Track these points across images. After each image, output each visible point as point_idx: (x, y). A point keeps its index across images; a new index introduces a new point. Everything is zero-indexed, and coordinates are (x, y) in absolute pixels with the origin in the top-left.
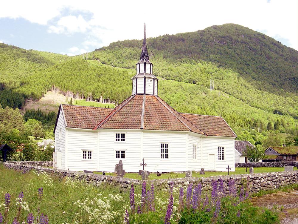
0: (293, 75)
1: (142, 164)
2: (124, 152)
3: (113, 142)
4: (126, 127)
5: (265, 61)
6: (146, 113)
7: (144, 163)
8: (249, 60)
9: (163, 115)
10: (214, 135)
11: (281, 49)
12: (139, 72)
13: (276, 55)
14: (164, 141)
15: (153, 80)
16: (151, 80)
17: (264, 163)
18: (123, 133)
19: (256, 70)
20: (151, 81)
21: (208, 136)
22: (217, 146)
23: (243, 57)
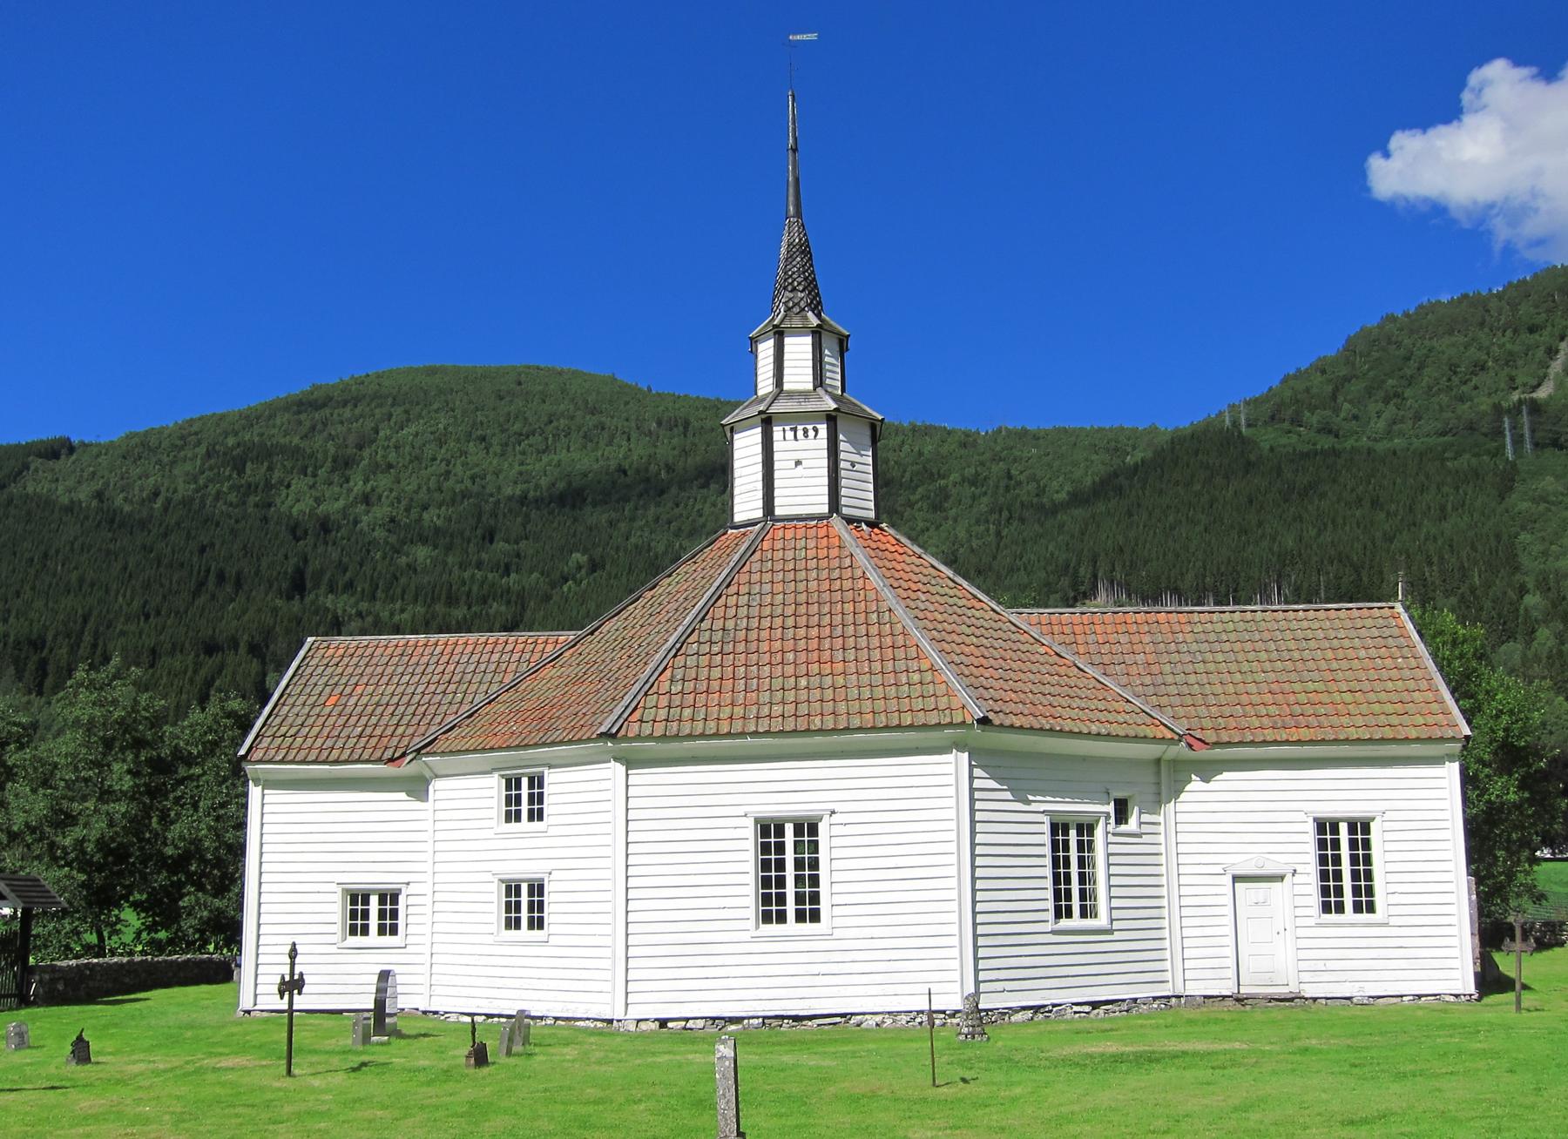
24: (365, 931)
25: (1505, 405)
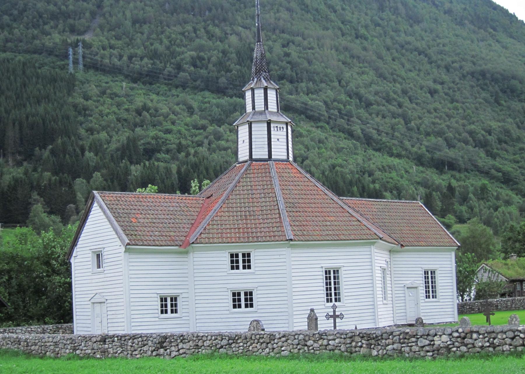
0: (480, 65)
1: (338, 316)
2: (251, 294)
3: (225, 274)
4: (253, 237)
5: (405, 27)
6: (288, 205)
7: (337, 313)
8: (366, 27)
9: (319, 205)
10: (416, 243)
12: (254, 108)
13: (434, 9)
15: (285, 126)
17: (497, 301)
18: (246, 251)
19: (384, 52)
20: (282, 129)
21: (406, 248)
23: (348, 16)
24: (166, 312)
25: (69, 41)
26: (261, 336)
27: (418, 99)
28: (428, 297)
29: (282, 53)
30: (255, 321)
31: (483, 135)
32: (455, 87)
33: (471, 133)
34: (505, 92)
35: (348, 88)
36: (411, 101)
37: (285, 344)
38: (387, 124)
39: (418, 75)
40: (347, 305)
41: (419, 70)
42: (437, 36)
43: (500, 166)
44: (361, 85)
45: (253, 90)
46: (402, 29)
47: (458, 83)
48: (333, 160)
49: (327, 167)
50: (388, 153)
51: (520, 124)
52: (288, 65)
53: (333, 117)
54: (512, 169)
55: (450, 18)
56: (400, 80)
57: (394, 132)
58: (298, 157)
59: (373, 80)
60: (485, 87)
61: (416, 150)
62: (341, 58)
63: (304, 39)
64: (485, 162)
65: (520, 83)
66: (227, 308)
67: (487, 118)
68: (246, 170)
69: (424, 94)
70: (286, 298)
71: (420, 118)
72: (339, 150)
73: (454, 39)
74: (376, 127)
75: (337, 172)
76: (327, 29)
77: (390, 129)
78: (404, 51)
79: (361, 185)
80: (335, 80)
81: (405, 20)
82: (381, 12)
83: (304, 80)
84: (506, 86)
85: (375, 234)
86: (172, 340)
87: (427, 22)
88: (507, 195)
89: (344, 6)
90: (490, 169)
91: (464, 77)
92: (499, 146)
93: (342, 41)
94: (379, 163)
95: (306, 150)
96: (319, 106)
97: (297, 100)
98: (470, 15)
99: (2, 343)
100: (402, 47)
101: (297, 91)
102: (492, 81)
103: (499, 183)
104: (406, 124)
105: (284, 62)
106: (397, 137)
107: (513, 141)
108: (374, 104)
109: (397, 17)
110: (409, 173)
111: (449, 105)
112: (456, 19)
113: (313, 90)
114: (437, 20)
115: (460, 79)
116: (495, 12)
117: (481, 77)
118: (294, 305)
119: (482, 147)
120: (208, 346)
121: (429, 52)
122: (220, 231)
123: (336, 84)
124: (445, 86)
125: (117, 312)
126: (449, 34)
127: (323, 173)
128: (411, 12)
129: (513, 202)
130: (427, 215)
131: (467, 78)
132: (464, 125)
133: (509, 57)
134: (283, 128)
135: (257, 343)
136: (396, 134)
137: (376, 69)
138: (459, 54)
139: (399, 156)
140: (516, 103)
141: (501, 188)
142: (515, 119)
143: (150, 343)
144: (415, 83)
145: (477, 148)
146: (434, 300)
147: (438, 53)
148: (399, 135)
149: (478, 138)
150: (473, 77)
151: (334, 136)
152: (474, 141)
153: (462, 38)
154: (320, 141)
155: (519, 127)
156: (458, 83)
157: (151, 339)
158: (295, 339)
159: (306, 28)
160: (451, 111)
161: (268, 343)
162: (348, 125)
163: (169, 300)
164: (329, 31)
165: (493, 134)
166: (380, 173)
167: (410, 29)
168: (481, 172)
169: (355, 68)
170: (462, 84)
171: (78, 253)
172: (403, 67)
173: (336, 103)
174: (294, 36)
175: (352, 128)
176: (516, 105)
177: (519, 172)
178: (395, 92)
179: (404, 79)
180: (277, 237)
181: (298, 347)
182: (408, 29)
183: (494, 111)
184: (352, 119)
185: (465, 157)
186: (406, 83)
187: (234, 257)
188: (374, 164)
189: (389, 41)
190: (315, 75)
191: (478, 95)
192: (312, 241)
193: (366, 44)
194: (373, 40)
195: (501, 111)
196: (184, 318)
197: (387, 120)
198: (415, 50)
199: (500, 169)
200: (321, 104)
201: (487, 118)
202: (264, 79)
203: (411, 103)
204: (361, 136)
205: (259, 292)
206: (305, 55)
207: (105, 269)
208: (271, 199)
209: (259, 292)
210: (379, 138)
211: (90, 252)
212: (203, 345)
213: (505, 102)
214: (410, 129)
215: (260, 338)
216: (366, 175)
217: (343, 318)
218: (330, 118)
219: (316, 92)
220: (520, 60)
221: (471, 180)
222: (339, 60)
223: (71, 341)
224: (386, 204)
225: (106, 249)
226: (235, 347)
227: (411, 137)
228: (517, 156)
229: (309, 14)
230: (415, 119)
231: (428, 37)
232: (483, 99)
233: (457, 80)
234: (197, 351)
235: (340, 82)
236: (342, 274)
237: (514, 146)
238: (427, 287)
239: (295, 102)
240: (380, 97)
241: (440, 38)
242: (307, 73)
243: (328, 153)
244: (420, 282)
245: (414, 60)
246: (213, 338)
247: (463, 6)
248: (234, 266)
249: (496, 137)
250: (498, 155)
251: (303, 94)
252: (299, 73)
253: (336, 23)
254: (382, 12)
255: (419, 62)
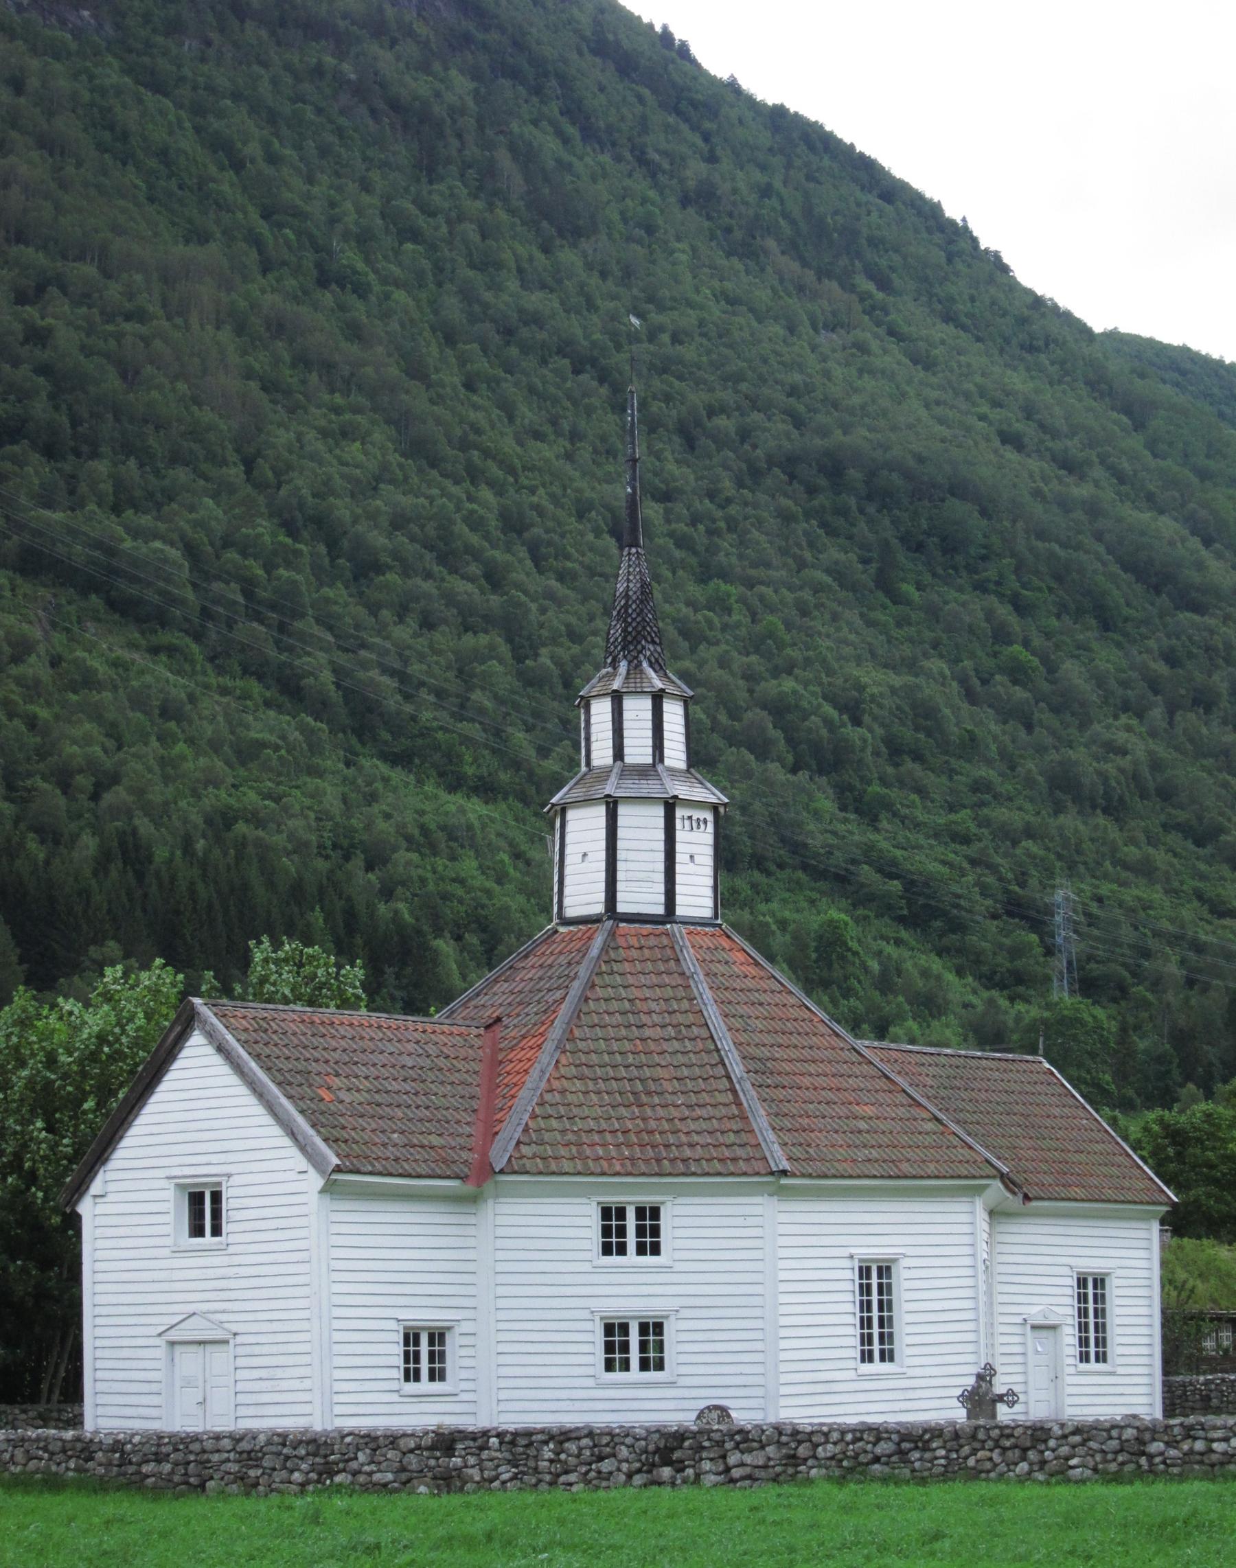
0: (823, 432)
2: (659, 1328)
4: (672, 1161)
5: (521, 250)
8: (363, 239)
11: (695, 128)
13: (640, 184)
14: (1092, 1265)
16: (698, 814)
17: (1207, 1383)
18: (647, 1199)
19: (431, 350)
21: (1034, 1204)
22: (1066, 1271)
26: (1007, 1431)
27: (568, 557)
28: (1085, 1358)
29: (18, 327)
30: (717, 1407)
31: (828, 722)
32: (719, 514)
33: (779, 709)
34: (919, 548)
35: (283, 492)
36: (537, 560)
37: (1081, 1450)
38: (438, 652)
39: (569, 457)
40: (910, 1372)
41: (575, 436)
42: (651, 299)
43: (899, 853)
44: (338, 482)
45: (617, 699)
46: (507, 256)
47: (729, 501)
48: (223, 794)
49: (196, 818)
50: (441, 774)
51: (975, 682)
52: (41, 380)
53: (221, 610)
54: (945, 870)
55: (707, 224)
56: (495, 471)
57: (471, 689)
58: (81, 771)
59: (385, 467)
60: (839, 522)
61: (556, 768)
62: (257, 366)
63: (107, 274)
64: (834, 833)
65: (984, 513)
66: (590, 1371)
67: (847, 650)
68: (605, 949)
69: (590, 537)
70: (759, 1346)
71: (575, 636)
72: (246, 753)
73: (716, 311)
74: (397, 665)
75: (241, 845)
76: (203, 238)
77: (450, 675)
78: (514, 351)
79: (340, 904)
80: (232, 457)
81: (524, 223)
82: (424, 180)
83: (104, 449)
84: (924, 525)
85: (987, 1161)
86: (706, 1444)
87: (609, 235)
88: (925, 973)
89: (276, 144)
90: (854, 862)
91: (755, 473)
92: (890, 770)
93: (263, 291)
94: (409, 817)
95: (111, 744)
96: (165, 560)
97: (72, 532)
98: (786, 215)
99: (7, 1456)
100: (508, 333)
101: (72, 492)
102: (869, 497)
103: (887, 919)
104: (520, 659)
105: (25, 370)
106: (481, 711)
107: (946, 753)
108: (390, 568)
109: (491, 207)
110: (528, 863)
111: (694, 590)
112: (728, 230)
113: (138, 493)
114: (650, 229)
115: (740, 484)
116: (888, 208)
117: (822, 482)
118: (783, 1368)
119: (821, 772)
120: (832, 1458)
121: (618, 359)
122: (570, 1137)
123: (235, 473)
124: (679, 508)
125: (279, 1373)
126: (698, 291)
127: (187, 844)
128: (547, 191)
129: (947, 1002)
130: (1071, 1101)
131: (769, 481)
132: (750, 677)
133: (938, 403)
134: (705, 822)
135: (991, 1450)
136: (477, 696)
137: (400, 421)
138: (736, 378)
139: (486, 789)
140: (965, 597)
141: (898, 942)
142: (958, 660)
143: (624, 1452)
144: (556, 489)
145: (803, 776)
146: (1101, 1367)
147: (652, 367)
148: (489, 704)
149: (810, 730)
150: (792, 477)
151: (224, 691)
152: (790, 741)
153: (751, 310)
154: (168, 711)
155: (970, 696)
156: (729, 501)
157: (629, 1441)
158: (1111, 1438)
159: (117, 229)
160: (699, 617)
161: (1027, 1449)
162: (281, 650)
163: (424, 1340)
164: (213, 247)
165: (866, 719)
166: (414, 856)
167: (539, 256)
168: (818, 874)
169: (313, 410)
170: (746, 504)
171: (112, 1187)
172: (511, 418)
173: (232, 555)
174: (64, 257)
175: (297, 662)
176: (964, 605)
177: (970, 878)
178: (475, 523)
179: (512, 471)
180: (741, 1163)
181: (1120, 1458)
182: (531, 259)
183: (870, 623)
184: (299, 625)
185: (757, 806)
186: (520, 488)
187: (611, 1216)
188: (388, 816)
189: (453, 307)
190: (149, 430)
191: (808, 555)
192: (835, 1177)
193: (359, 310)
194: (387, 296)
195: (899, 625)
196: (464, 1397)
197: (443, 637)
198: (560, 352)
199: (894, 862)
200: (175, 554)
201: (847, 650)
202: (651, 665)
203: (540, 571)
204: (334, 695)
205: (683, 1325)
206: (112, 343)
207: (231, 1239)
208: (700, 1045)
209: (683, 1325)
210: (408, 708)
211: (171, 1185)
212: (815, 1457)
213: (920, 587)
214: (531, 681)
215: (1002, 1436)
216: (358, 862)
217: (1014, 1402)
218: (206, 613)
219: (158, 501)
220: (982, 418)
221: (774, 905)
222: (249, 375)
223: (311, 1448)
224: (954, 1061)
225: (235, 1180)
226: (921, 1459)
227: (537, 714)
228: (965, 814)
229: (131, 168)
230: (554, 641)
231: (614, 297)
232: (828, 571)
233: (727, 486)
234: (791, 1470)
235: (249, 464)
236: (902, 1281)
237: (951, 773)
238: (1083, 1327)
239: (68, 539)
240: (413, 539)
241: (661, 308)
242: (117, 419)
243: (202, 761)
244: (1065, 1311)
245: (552, 390)
246: (849, 1437)
247: (758, 177)
248: (612, 1244)
249: (880, 731)
250: (888, 806)
251: (99, 505)
252: (86, 415)
253: (240, 215)
254: (431, 182)
255: (575, 403)
